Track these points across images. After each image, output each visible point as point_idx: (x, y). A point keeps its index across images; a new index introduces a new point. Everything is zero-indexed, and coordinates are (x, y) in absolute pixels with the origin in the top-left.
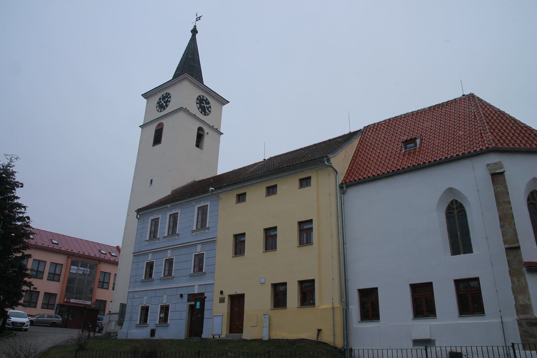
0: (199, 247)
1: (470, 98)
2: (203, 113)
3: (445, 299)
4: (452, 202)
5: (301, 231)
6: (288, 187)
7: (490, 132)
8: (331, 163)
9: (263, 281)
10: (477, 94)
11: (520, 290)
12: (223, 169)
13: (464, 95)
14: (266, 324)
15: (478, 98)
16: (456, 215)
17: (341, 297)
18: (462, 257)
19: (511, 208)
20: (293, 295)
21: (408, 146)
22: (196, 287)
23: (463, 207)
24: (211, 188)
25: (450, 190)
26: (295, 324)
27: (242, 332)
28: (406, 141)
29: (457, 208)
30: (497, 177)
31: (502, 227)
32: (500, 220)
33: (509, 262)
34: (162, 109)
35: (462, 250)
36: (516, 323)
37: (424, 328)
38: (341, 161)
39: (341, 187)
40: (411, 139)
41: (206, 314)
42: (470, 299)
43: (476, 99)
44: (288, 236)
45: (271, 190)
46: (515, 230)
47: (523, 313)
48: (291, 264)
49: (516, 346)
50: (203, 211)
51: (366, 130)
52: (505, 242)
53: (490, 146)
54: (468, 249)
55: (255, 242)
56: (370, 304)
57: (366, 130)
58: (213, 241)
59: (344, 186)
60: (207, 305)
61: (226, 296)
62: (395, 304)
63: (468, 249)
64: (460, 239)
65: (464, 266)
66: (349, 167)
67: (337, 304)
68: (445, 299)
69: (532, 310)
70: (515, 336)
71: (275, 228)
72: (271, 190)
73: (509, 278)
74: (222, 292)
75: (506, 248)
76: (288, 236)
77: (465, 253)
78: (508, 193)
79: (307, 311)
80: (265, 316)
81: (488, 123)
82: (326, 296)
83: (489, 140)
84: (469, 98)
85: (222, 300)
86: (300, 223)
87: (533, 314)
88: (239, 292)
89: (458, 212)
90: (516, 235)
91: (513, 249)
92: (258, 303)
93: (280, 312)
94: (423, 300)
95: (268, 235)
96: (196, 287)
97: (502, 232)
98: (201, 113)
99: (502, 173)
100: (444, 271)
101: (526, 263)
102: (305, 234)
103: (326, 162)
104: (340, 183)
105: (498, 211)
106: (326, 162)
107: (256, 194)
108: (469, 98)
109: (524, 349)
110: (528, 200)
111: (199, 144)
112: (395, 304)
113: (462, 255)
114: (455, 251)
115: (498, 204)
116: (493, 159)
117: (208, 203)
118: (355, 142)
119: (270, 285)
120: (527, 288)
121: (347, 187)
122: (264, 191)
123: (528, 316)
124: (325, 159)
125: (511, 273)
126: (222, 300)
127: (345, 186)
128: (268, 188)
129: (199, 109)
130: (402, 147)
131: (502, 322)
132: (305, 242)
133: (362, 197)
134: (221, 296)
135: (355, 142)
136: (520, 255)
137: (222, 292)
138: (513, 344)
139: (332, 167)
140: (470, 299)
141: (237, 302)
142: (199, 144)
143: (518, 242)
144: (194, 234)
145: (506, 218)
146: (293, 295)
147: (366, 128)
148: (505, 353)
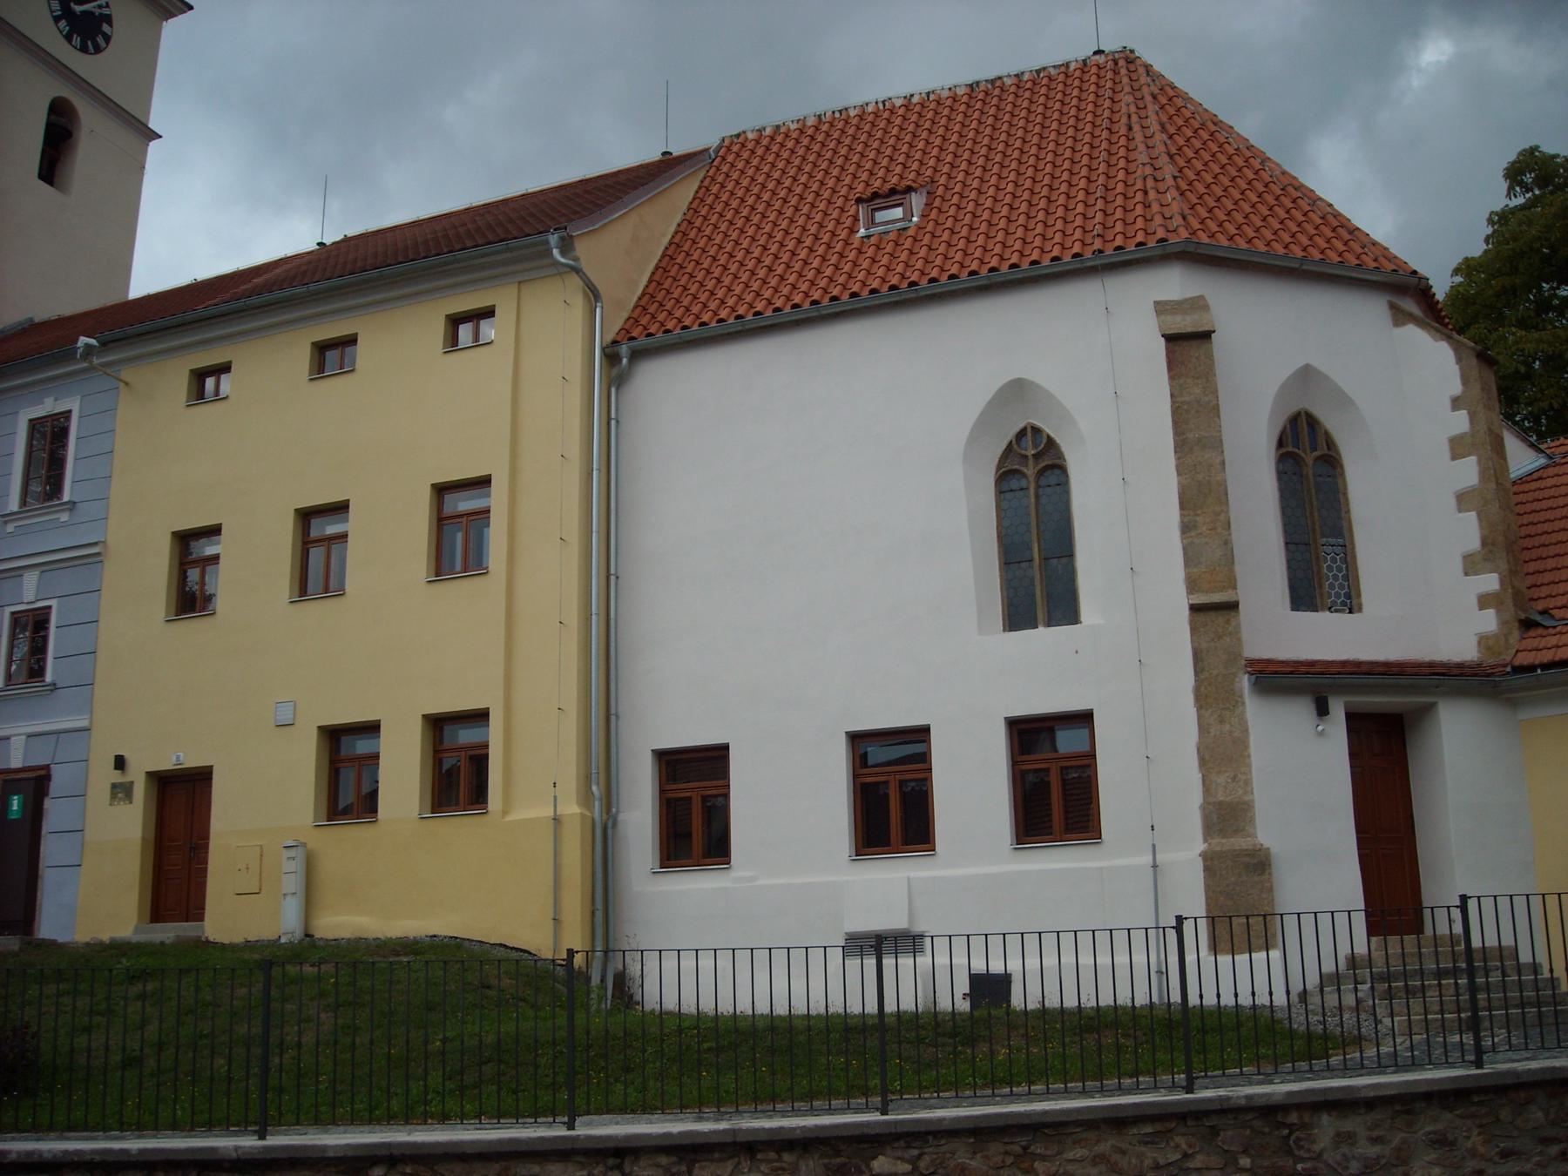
0: (30, 581)
1: (1122, 63)
2: (77, 40)
3: (972, 786)
4: (1021, 434)
5: (442, 521)
6: (397, 336)
7: (1178, 188)
8: (576, 259)
9: (285, 716)
10: (1147, 54)
11: (1222, 754)
12: (146, 280)
13: (1099, 52)
14: (292, 883)
15: (1148, 68)
16: (1030, 475)
17: (586, 779)
18: (1042, 636)
19: (1223, 463)
20: (402, 769)
21: (881, 216)
22: (18, 744)
23: (1060, 456)
24: (83, 340)
25: (1307, 375)
26: (418, 885)
27: (201, 918)
28: (875, 195)
29: (1036, 457)
30: (1187, 345)
31: (1186, 528)
32: (1182, 507)
33: (1197, 656)
34: (105, 28)
35: (1040, 615)
36: (1199, 865)
37: (886, 890)
38: (624, 252)
39: (611, 357)
40: (893, 191)
41: (52, 849)
42: (1054, 787)
43: (1141, 70)
44: (388, 538)
45: (331, 356)
46: (1227, 543)
47: (1223, 833)
48: (401, 648)
49: (1188, 927)
50: (50, 439)
51: (729, 149)
52: (1192, 585)
53: (1173, 239)
54: (1064, 609)
55: (254, 563)
56: (695, 807)
57: (729, 149)
58: (90, 558)
59: (624, 349)
60: (55, 813)
61: (137, 775)
62: (790, 803)
63: (1064, 609)
64: (1037, 579)
65: (1041, 671)
66: (650, 281)
67: (571, 808)
68: (972, 786)
69: (1252, 820)
70: (1190, 897)
71: (340, 509)
72: (332, 355)
73: (1192, 712)
74: (120, 763)
75: (1195, 609)
76: (388, 538)
77: (1049, 625)
78: (1216, 409)
79: (459, 828)
80: (293, 853)
81: (1171, 157)
82: (536, 776)
83: (1170, 213)
84: (1116, 62)
85: (122, 792)
86: (441, 490)
87: (1254, 835)
88: (192, 761)
89: (1041, 473)
90: (1230, 560)
91: (1213, 612)
92: (263, 800)
93: (352, 834)
94: (891, 798)
95: (314, 534)
96: (18, 744)
97: (1184, 548)
98: (68, 38)
99: (1206, 336)
100: (972, 691)
101: (1251, 662)
102: (459, 536)
103: (556, 252)
104: (609, 338)
105: (1179, 474)
106: (556, 252)
107: (269, 368)
108: (1116, 62)
109: (1215, 949)
110: (1281, 443)
111: (51, 169)
112: (790, 803)
113: (1041, 630)
114: (1018, 616)
115: (1182, 446)
116: (1173, 283)
117: (73, 404)
118: (683, 193)
119: (314, 733)
120: (1246, 746)
121: (637, 355)
122: (303, 356)
123: (1240, 843)
124: (553, 239)
125: (1201, 699)
126: (122, 792)
127: (623, 355)
128: (321, 349)
129: (57, 20)
130: (856, 219)
131: (1155, 866)
132: (458, 567)
133: (687, 393)
134: (117, 777)
135: (683, 193)
136: (1236, 634)
137: (120, 763)
138: (1180, 920)
139: (577, 271)
140: (1054, 787)
141: (181, 798)
142: (51, 169)
143: (1235, 587)
144: (10, 528)
145: (1202, 501)
146: (402, 769)
147: (736, 146)
148: (1154, 968)
